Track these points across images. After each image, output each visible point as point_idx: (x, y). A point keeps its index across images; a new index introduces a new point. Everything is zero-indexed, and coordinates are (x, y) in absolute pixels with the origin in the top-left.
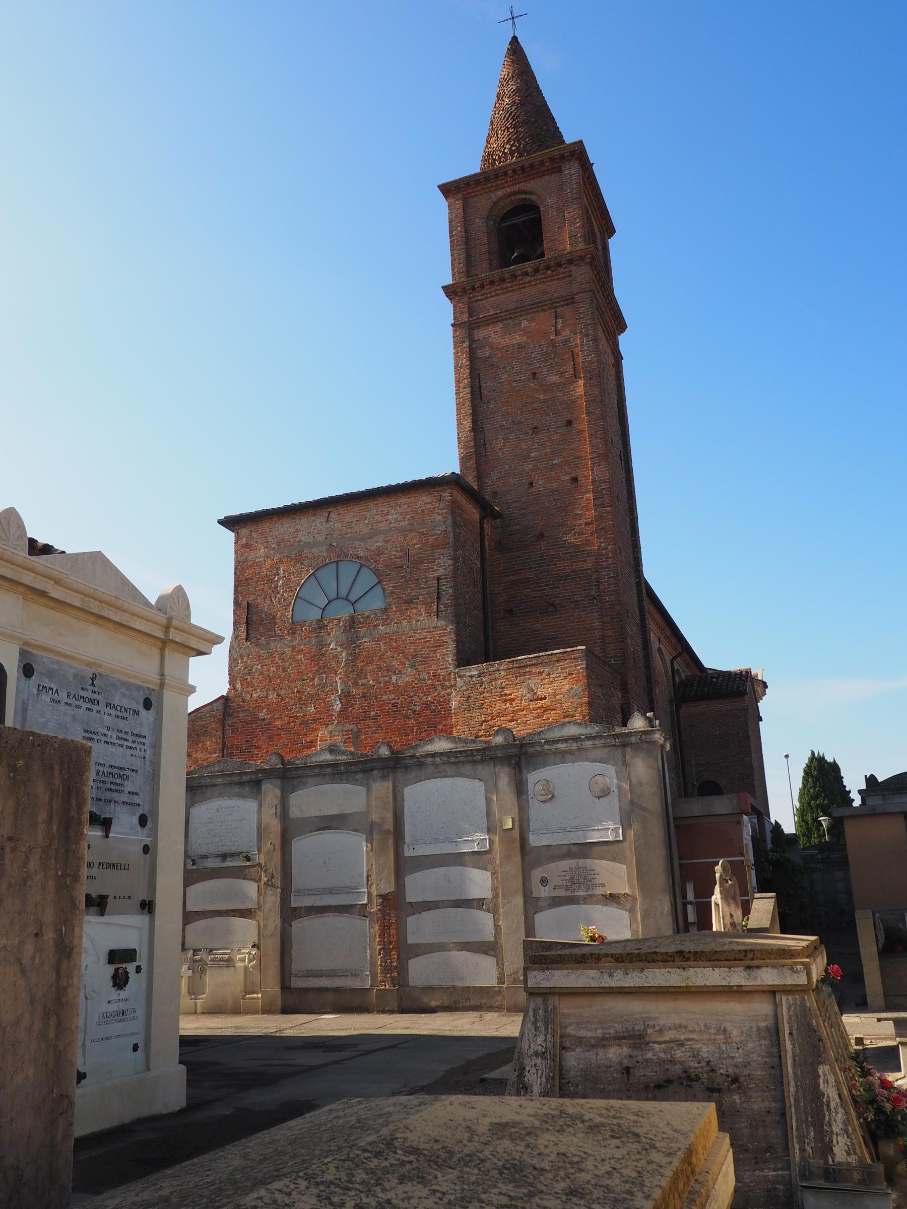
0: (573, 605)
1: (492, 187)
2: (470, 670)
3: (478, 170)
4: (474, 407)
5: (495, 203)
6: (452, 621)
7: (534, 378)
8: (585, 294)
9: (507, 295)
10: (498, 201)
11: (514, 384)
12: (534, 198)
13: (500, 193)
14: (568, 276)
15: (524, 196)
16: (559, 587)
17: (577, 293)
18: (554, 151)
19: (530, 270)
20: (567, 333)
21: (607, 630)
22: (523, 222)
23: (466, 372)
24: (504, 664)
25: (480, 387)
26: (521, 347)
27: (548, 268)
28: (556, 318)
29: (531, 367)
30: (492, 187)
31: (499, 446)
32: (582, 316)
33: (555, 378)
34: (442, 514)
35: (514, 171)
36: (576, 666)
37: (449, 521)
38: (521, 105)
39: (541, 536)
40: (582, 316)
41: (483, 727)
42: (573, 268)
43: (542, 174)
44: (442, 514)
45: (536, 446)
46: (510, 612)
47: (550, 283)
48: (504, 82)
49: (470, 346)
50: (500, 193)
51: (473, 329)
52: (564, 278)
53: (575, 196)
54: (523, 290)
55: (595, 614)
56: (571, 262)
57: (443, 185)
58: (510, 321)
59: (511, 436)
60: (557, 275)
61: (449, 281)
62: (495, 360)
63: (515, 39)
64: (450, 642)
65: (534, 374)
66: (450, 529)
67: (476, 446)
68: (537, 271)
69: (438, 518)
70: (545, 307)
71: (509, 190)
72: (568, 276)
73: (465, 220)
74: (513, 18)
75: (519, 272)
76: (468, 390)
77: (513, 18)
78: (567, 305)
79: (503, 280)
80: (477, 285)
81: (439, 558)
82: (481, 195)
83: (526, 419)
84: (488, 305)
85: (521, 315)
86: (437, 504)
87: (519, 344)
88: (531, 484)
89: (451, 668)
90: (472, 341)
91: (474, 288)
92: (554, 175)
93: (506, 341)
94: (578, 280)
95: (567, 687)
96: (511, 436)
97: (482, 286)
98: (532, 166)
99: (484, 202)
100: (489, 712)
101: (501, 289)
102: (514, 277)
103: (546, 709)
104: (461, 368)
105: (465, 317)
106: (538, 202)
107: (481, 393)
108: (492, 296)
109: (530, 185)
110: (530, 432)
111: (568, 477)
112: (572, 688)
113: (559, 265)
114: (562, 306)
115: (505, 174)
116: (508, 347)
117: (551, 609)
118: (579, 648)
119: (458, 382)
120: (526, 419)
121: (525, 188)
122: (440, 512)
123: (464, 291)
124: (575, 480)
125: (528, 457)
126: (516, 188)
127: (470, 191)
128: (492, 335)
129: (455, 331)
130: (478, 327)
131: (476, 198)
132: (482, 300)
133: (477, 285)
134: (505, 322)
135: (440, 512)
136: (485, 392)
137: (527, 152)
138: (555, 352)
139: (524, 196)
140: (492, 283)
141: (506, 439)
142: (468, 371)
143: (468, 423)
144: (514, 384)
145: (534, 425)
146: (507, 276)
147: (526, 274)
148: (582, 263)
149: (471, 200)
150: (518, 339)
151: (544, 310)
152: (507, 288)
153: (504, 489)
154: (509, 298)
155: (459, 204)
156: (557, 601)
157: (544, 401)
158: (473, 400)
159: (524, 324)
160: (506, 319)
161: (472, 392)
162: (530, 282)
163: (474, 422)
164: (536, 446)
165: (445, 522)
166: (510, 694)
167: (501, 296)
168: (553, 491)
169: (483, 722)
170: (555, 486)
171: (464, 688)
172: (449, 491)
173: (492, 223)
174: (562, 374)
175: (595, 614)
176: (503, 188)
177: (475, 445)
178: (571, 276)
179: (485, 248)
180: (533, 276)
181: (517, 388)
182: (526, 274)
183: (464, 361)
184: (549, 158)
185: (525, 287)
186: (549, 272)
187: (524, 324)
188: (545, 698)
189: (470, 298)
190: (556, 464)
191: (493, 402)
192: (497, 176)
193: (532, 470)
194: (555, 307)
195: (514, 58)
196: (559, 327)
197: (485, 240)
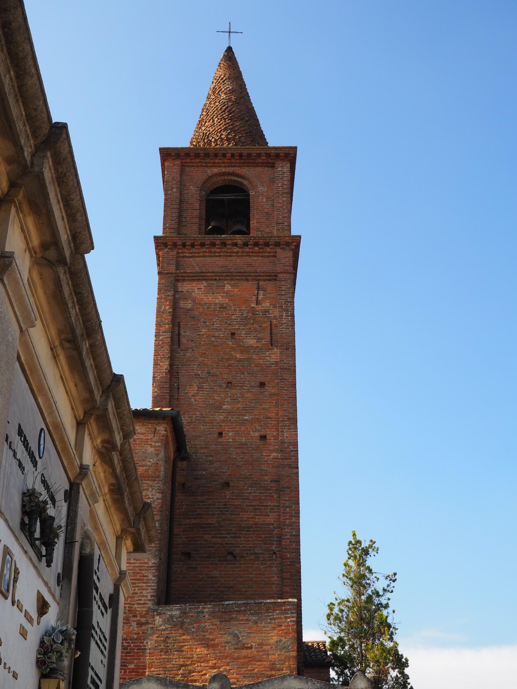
0: (252, 557)
1: (209, 163)
2: (171, 610)
3: (187, 145)
4: (172, 351)
5: (210, 178)
6: (156, 556)
7: (232, 338)
8: (288, 275)
9: (213, 259)
10: (213, 176)
11: (213, 339)
12: (245, 182)
13: (216, 170)
14: (272, 256)
15: (236, 179)
16: (240, 537)
17: (281, 273)
18: (255, 149)
19: (240, 242)
20: (266, 304)
21: (286, 586)
22: (229, 200)
23: (168, 318)
24: (208, 608)
25: (179, 334)
26: (222, 307)
27: (256, 244)
28: (258, 289)
29: (230, 327)
30: (209, 163)
31: (192, 392)
32: (283, 293)
33: (252, 342)
34: (154, 447)
35: (233, 155)
36: (286, 618)
37: (162, 455)
38: (236, 103)
39: (227, 484)
40: (283, 293)
41: (181, 672)
42: (279, 250)
43: (257, 165)
44: (154, 447)
45: (228, 399)
46: (188, 555)
47: (255, 258)
48: (218, 80)
49: (174, 295)
50: (216, 170)
51: (178, 280)
52: (269, 256)
53: (285, 191)
54: (229, 258)
55: (274, 569)
56: (278, 244)
57: (164, 149)
58: (214, 282)
59: (205, 386)
60: (263, 252)
61: (160, 233)
62: (197, 313)
63: (229, 49)
64: (151, 577)
65: (233, 334)
66: (161, 463)
67: (171, 388)
68: (246, 244)
69: (150, 450)
70: (250, 278)
71: (224, 170)
72: (272, 256)
73: (181, 184)
74: (230, 32)
75: (229, 242)
76: (169, 335)
77: (230, 32)
78: (269, 280)
79: (213, 245)
80: (188, 243)
81: (147, 490)
82: (197, 166)
83: (221, 373)
84: (194, 263)
85: (226, 280)
86: (150, 436)
87: (221, 305)
88: (220, 434)
89: (150, 604)
90: (176, 291)
91: (184, 245)
92: (266, 168)
93: (209, 299)
94: (283, 261)
95: (275, 638)
96: (205, 386)
97: (193, 245)
98: (249, 155)
99: (200, 175)
100: (189, 656)
101: (210, 252)
102: (224, 244)
103: (253, 659)
104: (163, 313)
105: (172, 268)
106: (249, 186)
107: (179, 340)
108: (200, 256)
109: (244, 171)
110: (224, 385)
111: (257, 434)
112: (280, 641)
113: (267, 245)
114: (265, 280)
115: (224, 155)
116: (210, 304)
117: (230, 557)
118: (290, 600)
119: (158, 325)
120: (221, 373)
121: (239, 172)
122: (153, 444)
123: (175, 245)
124: (263, 438)
125: (220, 408)
126: (228, 170)
127: (189, 161)
128: (196, 290)
129: (160, 279)
130: (183, 280)
131: (192, 168)
132: (189, 257)
133: (188, 243)
134: (209, 282)
135: (153, 444)
136: (183, 340)
137: (242, 143)
138: (254, 319)
139: (236, 179)
140: (203, 245)
141: (200, 388)
142: (170, 317)
143: (165, 365)
144: (213, 339)
145: (229, 380)
146: (218, 242)
147: (236, 245)
148: (287, 248)
149: (187, 169)
150: (220, 299)
151: (247, 280)
152: (215, 252)
153: (194, 434)
154: (215, 262)
155: (176, 169)
156: (237, 551)
157: (240, 360)
158: (172, 345)
159: (228, 287)
160: (211, 280)
161: (172, 338)
162: (237, 252)
163: (171, 365)
164: (228, 399)
165: (157, 455)
166: (213, 640)
167: (208, 259)
168: (241, 444)
169: (182, 666)
170: (244, 440)
171: (163, 627)
172: (165, 425)
173: (204, 193)
174: (259, 339)
175: (274, 569)
176: (219, 167)
177: (169, 387)
178: (275, 256)
179: (196, 213)
180: (242, 248)
181: (215, 343)
182: (236, 245)
183: (167, 307)
184: (266, 154)
185: (231, 256)
186: (256, 248)
187: (228, 287)
188: (251, 648)
189: (178, 253)
190: (247, 420)
191: (190, 350)
192: (216, 155)
193: (223, 421)
194: (258, 280)
195: (230, 64)
196: (260, 297)
197: (197, 206)
